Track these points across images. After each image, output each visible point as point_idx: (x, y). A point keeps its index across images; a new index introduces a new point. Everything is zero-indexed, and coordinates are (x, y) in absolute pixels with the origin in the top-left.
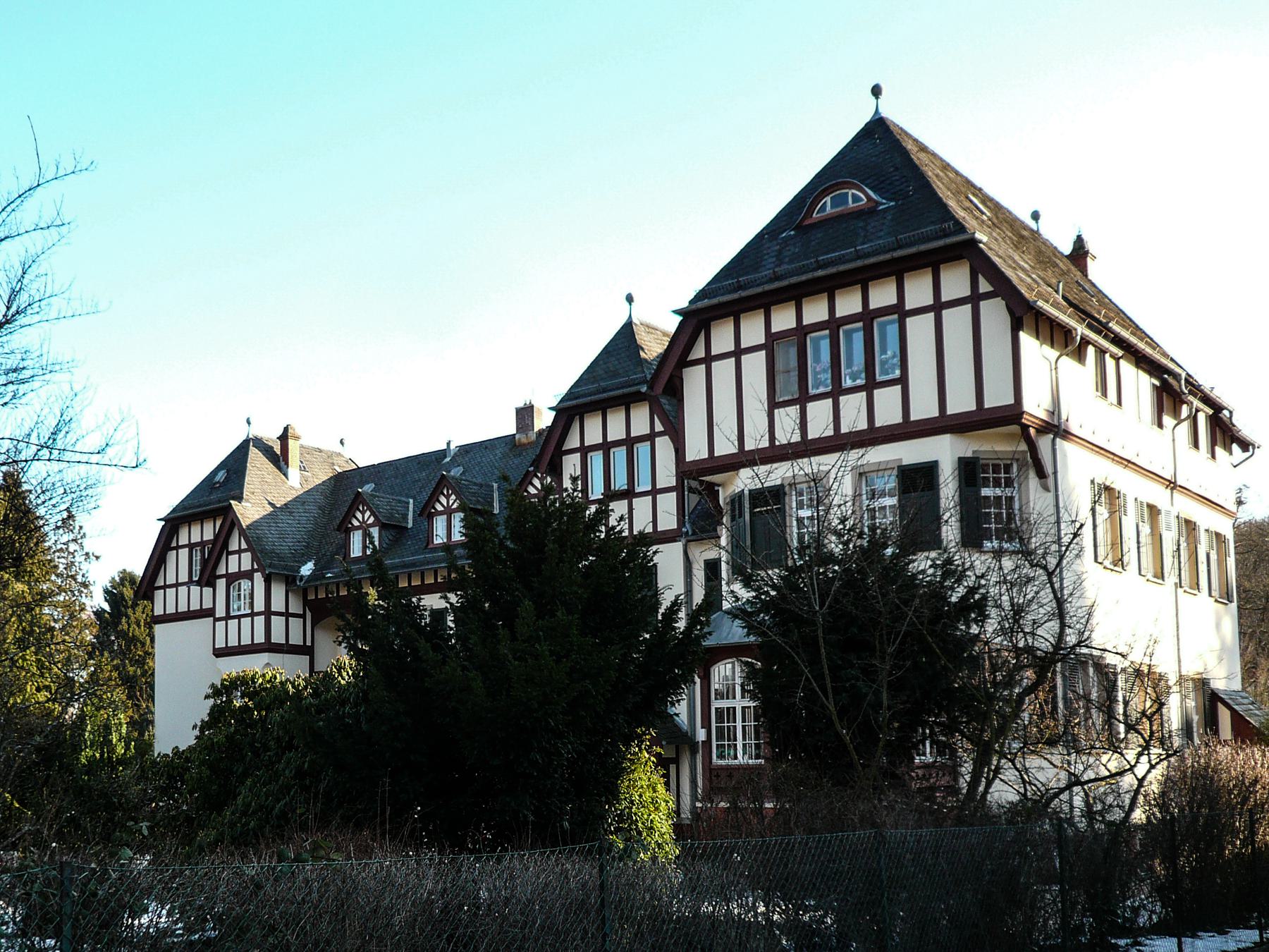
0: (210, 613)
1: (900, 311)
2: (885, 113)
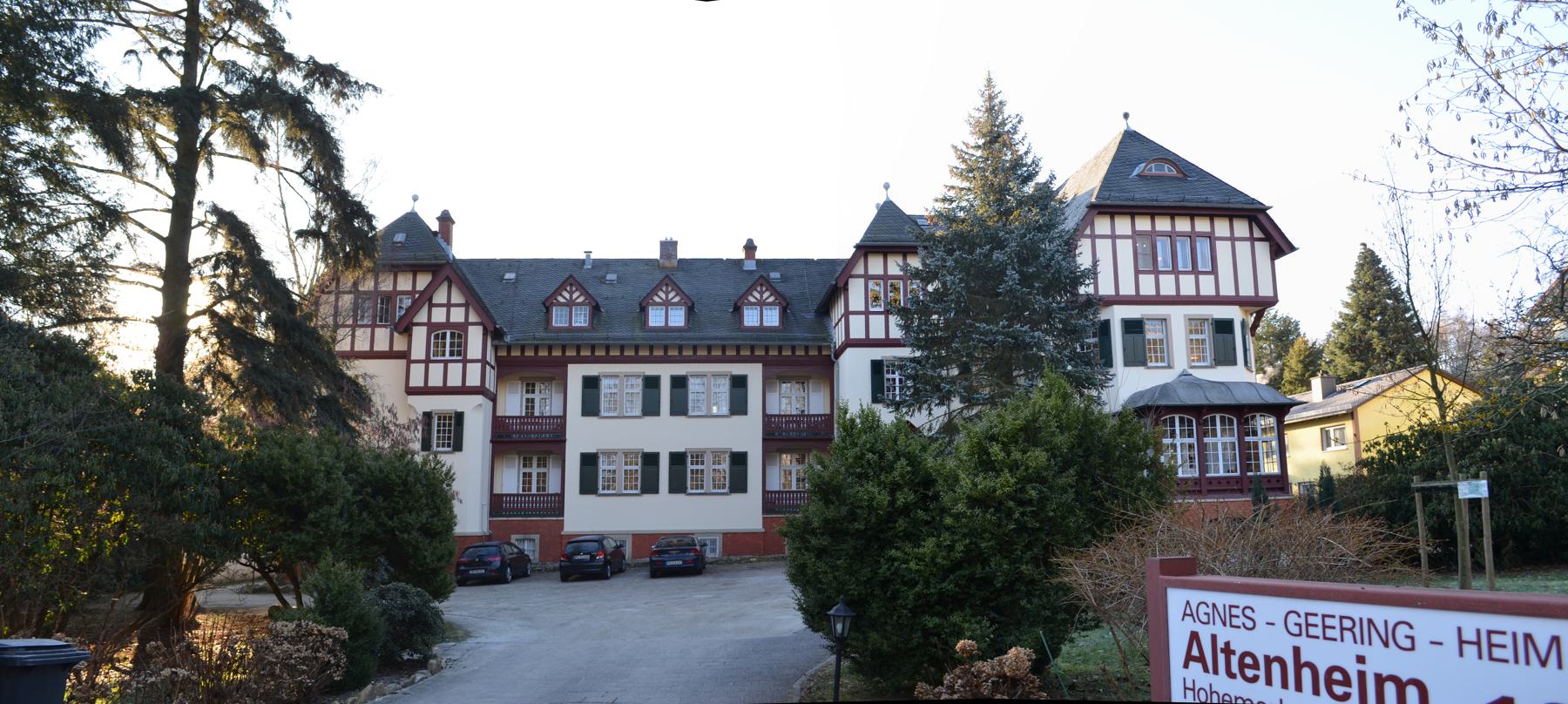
0: (405, 355)
1: (1211, 237)
2: (1134, 127)
